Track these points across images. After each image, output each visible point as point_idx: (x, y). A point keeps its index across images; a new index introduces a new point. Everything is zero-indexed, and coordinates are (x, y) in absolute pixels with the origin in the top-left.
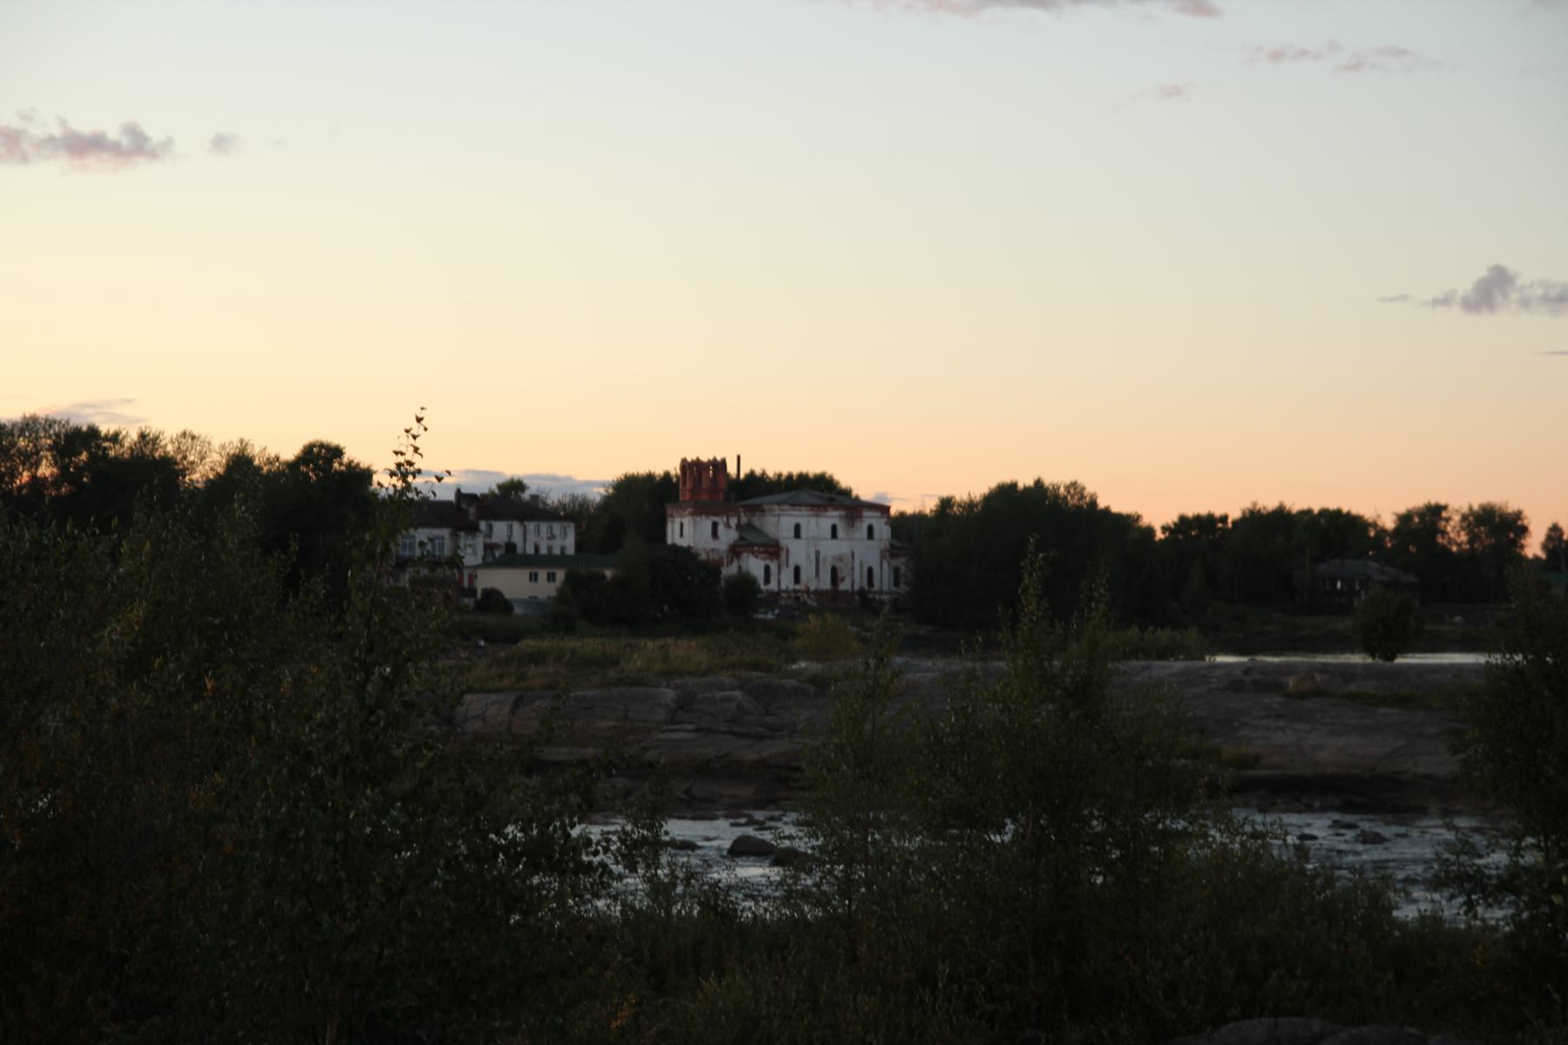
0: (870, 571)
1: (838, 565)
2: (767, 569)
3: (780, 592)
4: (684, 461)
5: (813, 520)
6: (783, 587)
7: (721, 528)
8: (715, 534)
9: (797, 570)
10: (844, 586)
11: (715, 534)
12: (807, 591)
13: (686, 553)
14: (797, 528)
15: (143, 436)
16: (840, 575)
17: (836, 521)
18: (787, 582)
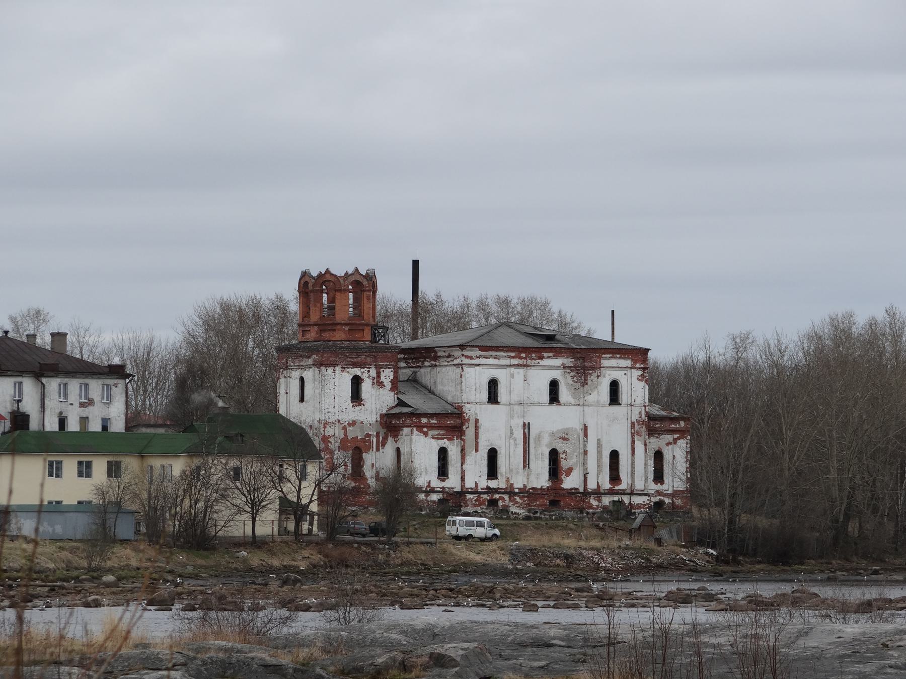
0: (614, 455)
1: (561, 446)
2: (443, 454)
3: (462, 493)
7: (367, 387)
8: (356, 397)
9: (493, 455)
10: (570, 482)
11: (356, 397)
12: (510, 491)
14: (493, 385)
16: (564, 464)
17: (557, 374)
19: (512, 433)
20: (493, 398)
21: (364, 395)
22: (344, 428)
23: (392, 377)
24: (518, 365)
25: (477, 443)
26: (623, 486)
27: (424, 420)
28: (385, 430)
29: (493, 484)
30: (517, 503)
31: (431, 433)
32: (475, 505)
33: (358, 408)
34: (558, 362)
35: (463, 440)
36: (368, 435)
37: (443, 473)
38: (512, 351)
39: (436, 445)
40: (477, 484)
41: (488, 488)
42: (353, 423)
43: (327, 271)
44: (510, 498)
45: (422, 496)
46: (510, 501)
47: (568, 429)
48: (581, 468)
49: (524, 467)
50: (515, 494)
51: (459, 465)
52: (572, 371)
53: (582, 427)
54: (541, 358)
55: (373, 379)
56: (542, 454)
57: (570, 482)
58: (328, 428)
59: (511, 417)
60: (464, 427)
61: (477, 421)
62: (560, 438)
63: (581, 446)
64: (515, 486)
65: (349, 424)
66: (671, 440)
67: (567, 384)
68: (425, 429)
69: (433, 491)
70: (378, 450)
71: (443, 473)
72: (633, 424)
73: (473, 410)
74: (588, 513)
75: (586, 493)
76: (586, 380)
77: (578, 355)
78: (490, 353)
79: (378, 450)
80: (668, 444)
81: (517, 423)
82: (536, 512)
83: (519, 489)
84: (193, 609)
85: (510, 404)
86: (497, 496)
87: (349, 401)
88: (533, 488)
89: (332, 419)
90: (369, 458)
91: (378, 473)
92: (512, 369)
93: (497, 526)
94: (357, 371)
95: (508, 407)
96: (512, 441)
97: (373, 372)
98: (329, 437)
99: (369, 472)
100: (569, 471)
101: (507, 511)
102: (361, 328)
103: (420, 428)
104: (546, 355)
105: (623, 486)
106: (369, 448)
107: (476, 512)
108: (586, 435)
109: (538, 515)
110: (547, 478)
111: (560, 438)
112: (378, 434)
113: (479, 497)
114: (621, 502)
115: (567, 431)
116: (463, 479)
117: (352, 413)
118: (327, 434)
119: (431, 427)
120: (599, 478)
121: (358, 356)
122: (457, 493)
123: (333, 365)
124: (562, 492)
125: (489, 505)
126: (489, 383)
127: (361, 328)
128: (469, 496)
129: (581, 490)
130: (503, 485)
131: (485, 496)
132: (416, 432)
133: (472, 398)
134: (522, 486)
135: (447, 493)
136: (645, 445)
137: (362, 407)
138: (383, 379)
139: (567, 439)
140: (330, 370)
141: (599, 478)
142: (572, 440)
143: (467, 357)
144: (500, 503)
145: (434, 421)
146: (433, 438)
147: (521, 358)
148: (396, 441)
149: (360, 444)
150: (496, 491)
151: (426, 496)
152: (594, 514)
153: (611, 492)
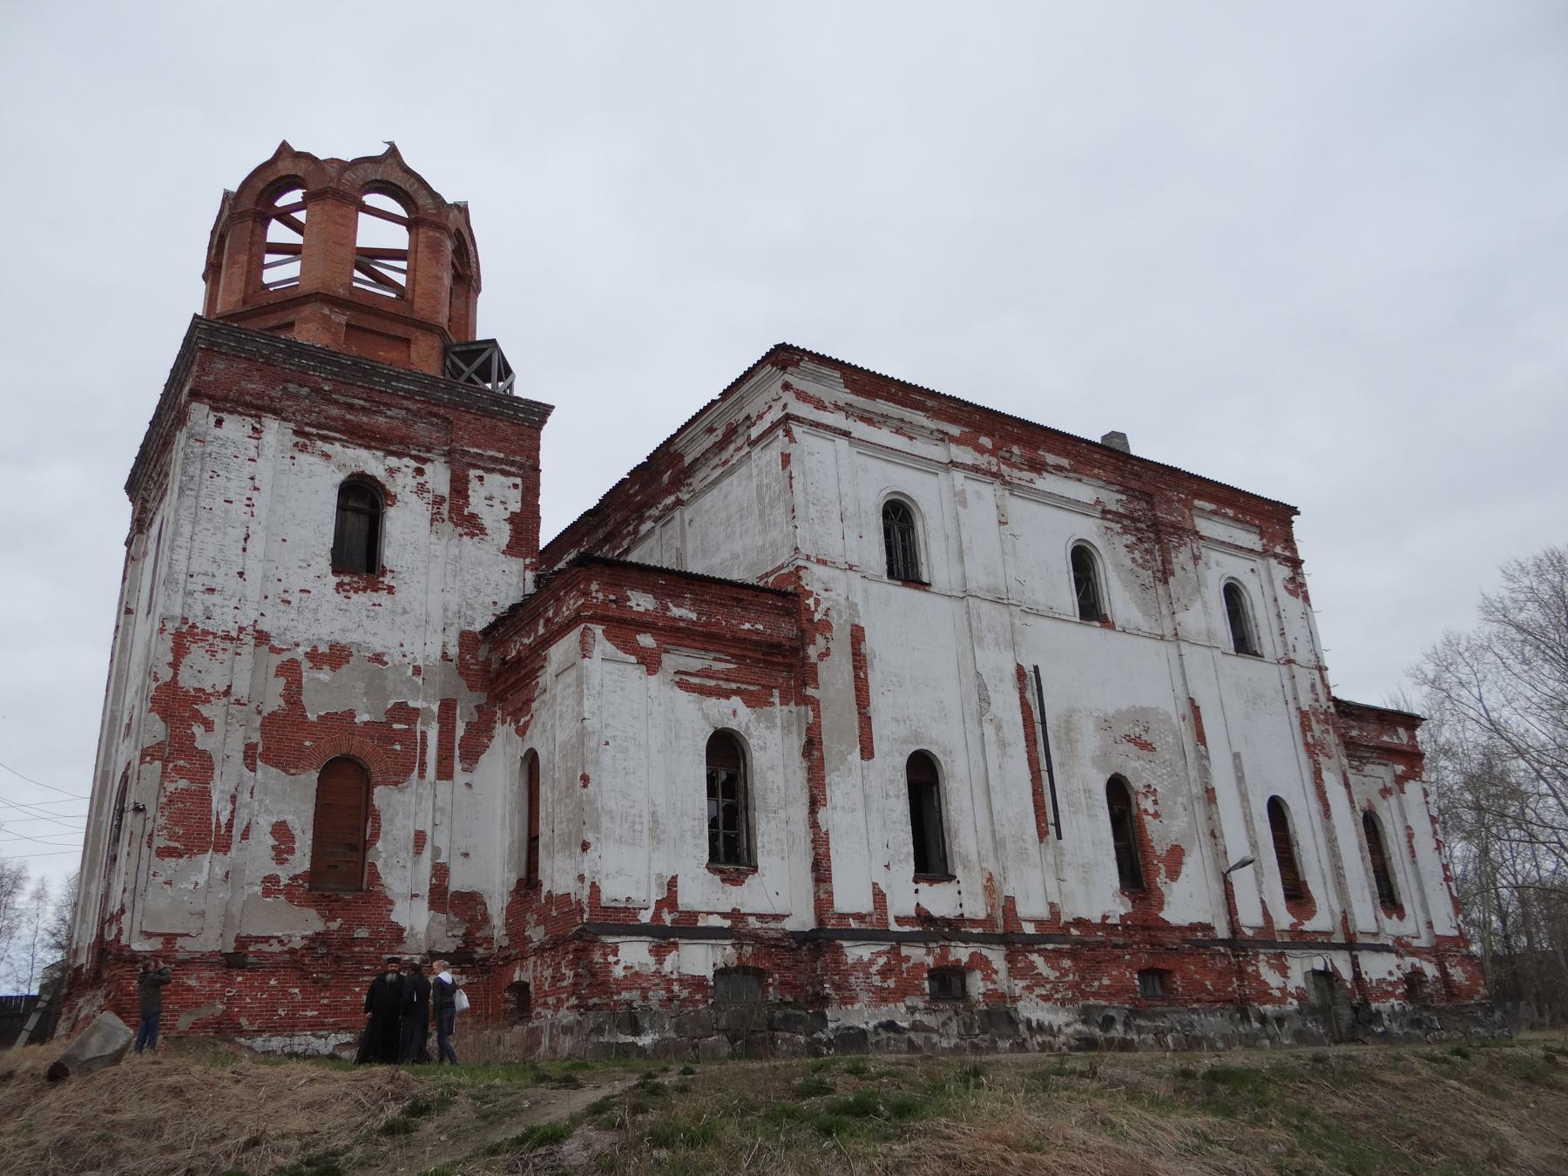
0: (1277, 809)
1: (1138, 771)
2: (726, 753)
3: (823, 939)
4: (540, 412)
5: (984, 495)
6: (850, 897)
7: (406, 528)
8: (359, 553)
9: (923, 775)
10: (1187, 901)
11: (359, 553)
12: (1006, 932)
13: (366, 723)
14: (898, 518)
15: (332, 647)
16: (1160, 833)
17: (1088, 529)
18: (872, 864)
19: (984, 699)
20: (903, 564)
21: (390, 554)
22: (290, 670)
23: (516, 507)
24: (976, 469)
25: (865, 721)
26: (1321, 921)
27: (641, 602)
28: (481, 698)
29: (939, 900)
30: (1040, 981)
31: (674, 661)
32: (882, 996)
33: (361, 599)
34: (1084, 492)
35: (814, 703)
36: (404, 712)
37: (731, 848)
38: (953, 420)
39: (697, 718)
40: (879, 897)
41: (923, 917)
42: (337, 656)
43: (284, 148)
44: (1010, 958)
45: (633, 954)
46: (1014, 972)
47: (1144, 710)
48: (1207, 852)
49: (1042, 834)
50: (1030, 943)
51: (800, 811)
52: (1126, 530)
53: (1185, 709)
54: (1038, 467)
55: (438, 501)
56: (1088, 791)
57: (1187, 901)
58: (197, 654)
59: (973, 637)
60: (812, 652)
61: (857, 635)
62: (1130, 739)
63: (1193, 774)
64: (1023, 910)
65: (313, 656)
66: (1389, 781)
67: (1119, 566)
68: (646, 640)
69: (689, 928)
70: (445, 773)
71: (731, 848)
72: (1304, 715)
73: (839, 590)
74: (1263, 1019)
75: (1237, 942)
76: (1166, 561)
77: (1134, 484)
78: (881, 406)
79: (445, 773)
80: (1385, 792)
81: (998, 664)
82: (1108, 1023)
83: (1038, 923)
84: (1458, 905)
85: (966, 595)
86: (961, 953)
87: (324, 564)
88: (1079, 923)
89: (225, 620)
90: (401, 810)
91: (440, 872)
92: (958, 476)
93: (1523, 902)
94: (372, 463)
95: (958, 607)
96: (989, 730)
97: (438, 477)
98: (202, 696)
99: (401, 878)
100: (1175, 858)
101: (1011, 1020)
102: (400, 331)
103: (622, 628)
104: (1051, 459)
105: (1321, 921)
106: (403, 768)
107: (890, 1026)
108: (1201, 737)
109: (1118, 1032)
110: (1115, 882)
111: (1130, 739)
112: (447, 707)
113: (894, 953)
114: (1326, 977)
115: (1141, 716)
116: (821, 871)
117: (328, 613)
118: (187, 681)
119: (676, 635)
120: (1259, 898)
121: (377, 405)
122: (801, 937)
123: (256, 408)
124: (1172, 940)
125: (935, 997)
126: (886, 514)
127: (400, 331)
128: (856, 952)
129: (1222, 932)
130: (976, 908)
131: (917, 953)
132: (602, 645)
133: (833, 547)
134: (1042, 912)
135: (755, 937)
136: (1347, 785)
137: (382, 597)
138: (476, 502)
139: (1146, 746)
140: (235, 428)
141: (1259, 898)
142: (1163, 742)
143: (802, 396)
144: (977, 985)
145: (683, 612)
146: (683, 685)
147: (981, 450)
148: (521, 731)
149: (363, 748)
150: (953, 929)
151: (659, 953)
152: (1280, 1020)
153: (1303, 941)
